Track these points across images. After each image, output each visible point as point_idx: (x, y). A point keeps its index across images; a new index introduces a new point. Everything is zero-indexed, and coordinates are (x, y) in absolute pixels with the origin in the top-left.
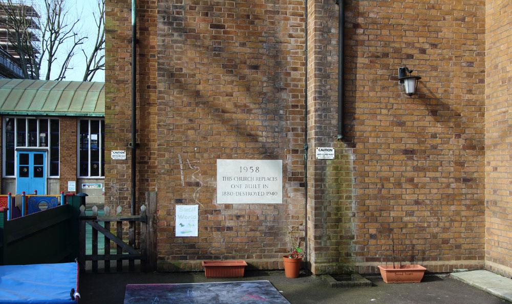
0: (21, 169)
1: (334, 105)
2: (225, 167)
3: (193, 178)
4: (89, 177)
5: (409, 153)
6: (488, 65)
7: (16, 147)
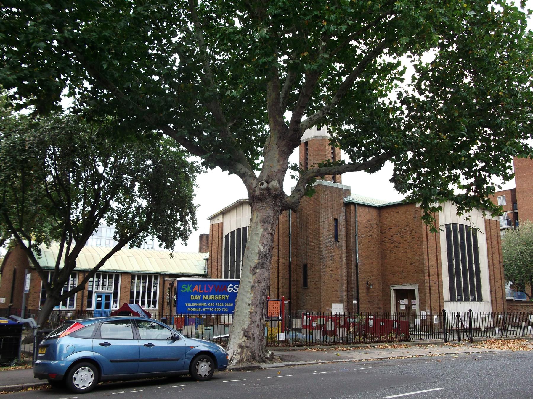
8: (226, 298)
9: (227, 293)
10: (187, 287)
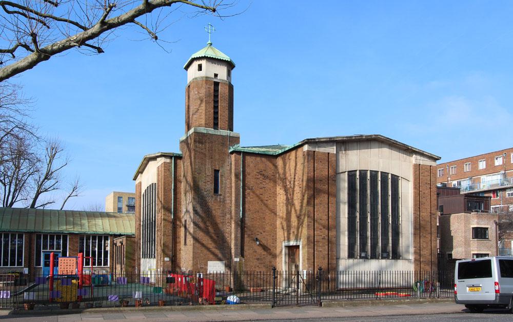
0: (54, 262)
1: (239, 247)
2: (210, 263)
3: (202, 266)
4: (96, 266)
5: (258, 259)
6: (277, 237)
7: (42, 250)
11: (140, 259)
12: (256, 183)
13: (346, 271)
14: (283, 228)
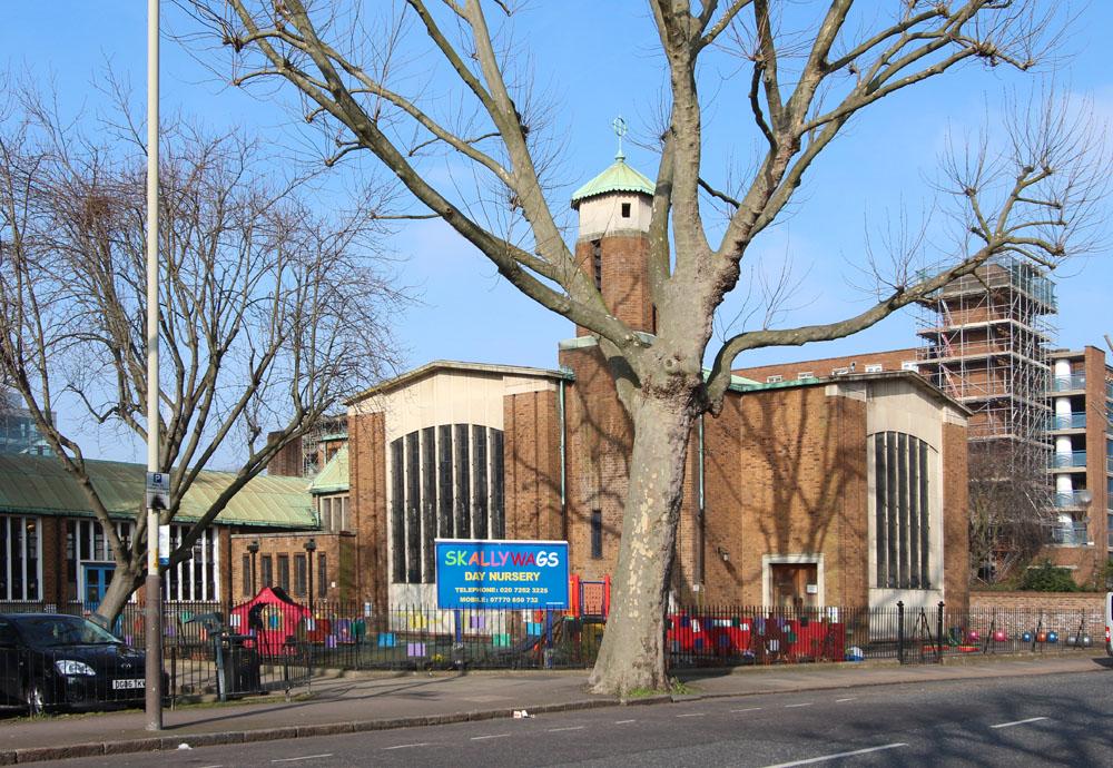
1: (699, 565)
5: (721, 587)
8: (534, 577)
9: (538, 569)
10: (456, 556)
11: (386, 585)
12: (717, 443)
13: (878, 611)
14: (764, 530)
